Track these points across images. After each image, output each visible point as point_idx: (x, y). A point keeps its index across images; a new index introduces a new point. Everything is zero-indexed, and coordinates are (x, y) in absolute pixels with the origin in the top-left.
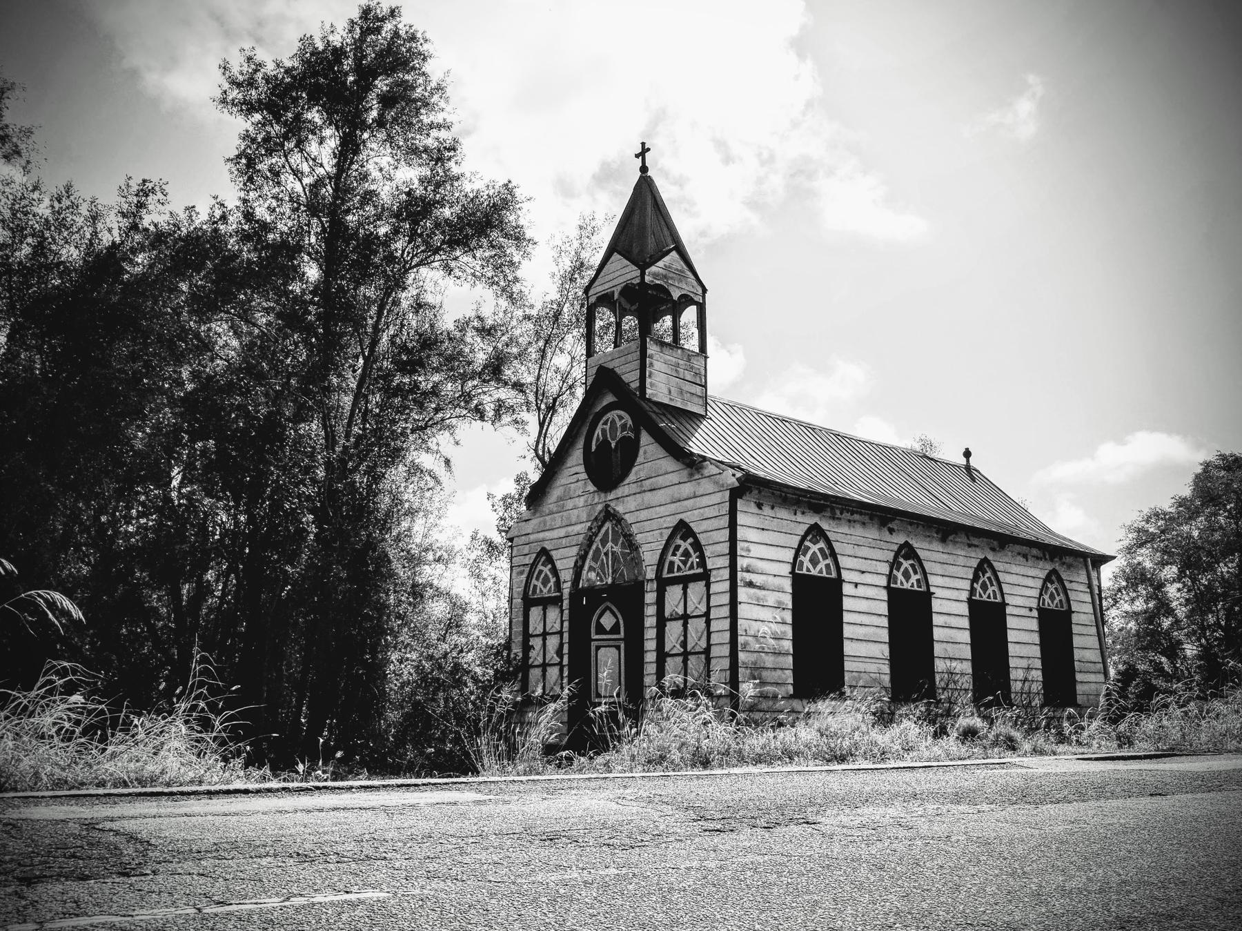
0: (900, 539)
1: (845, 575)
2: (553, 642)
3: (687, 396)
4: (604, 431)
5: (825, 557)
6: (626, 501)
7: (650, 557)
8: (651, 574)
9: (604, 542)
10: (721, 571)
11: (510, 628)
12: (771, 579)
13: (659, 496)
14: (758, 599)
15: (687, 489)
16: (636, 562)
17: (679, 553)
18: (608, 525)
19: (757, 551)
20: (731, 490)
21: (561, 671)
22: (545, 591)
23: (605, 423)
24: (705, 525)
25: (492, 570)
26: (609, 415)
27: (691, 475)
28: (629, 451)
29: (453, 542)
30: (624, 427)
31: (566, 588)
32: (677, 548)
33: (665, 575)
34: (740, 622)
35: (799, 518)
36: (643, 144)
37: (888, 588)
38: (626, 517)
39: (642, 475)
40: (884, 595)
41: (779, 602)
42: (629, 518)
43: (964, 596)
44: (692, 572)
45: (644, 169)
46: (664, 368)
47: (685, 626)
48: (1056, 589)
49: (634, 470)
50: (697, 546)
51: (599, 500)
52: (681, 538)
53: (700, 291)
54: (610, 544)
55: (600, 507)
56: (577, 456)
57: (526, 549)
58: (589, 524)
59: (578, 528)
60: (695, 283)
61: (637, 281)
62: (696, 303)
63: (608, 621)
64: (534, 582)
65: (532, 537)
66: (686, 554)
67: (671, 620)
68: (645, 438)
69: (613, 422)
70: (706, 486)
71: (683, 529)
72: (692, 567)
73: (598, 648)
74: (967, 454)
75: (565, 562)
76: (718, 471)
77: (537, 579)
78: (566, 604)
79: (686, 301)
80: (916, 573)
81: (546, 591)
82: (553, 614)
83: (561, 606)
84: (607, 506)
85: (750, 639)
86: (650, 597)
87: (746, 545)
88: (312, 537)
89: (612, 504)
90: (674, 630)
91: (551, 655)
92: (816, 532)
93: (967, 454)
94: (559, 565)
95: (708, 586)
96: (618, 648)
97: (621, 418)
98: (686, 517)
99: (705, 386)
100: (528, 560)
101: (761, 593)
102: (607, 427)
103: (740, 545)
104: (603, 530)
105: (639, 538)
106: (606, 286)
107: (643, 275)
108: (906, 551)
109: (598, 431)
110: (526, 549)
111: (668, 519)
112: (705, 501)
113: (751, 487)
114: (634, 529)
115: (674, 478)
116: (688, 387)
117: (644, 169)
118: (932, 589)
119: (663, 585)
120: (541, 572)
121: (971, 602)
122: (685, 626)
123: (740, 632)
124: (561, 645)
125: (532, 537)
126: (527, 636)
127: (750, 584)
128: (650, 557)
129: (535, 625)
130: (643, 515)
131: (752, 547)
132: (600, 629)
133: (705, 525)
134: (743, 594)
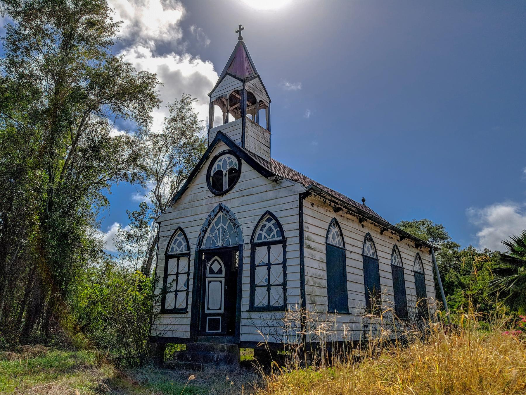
0: (366, 231)
1: (348, 247)
2: (183, 279)
3: (262, 151)
4: (219, 165)
5: (338, 236)
6: (231, 200)
7: (246, 232)
8: (247, 240)
9: (217, 223)
10: (293, 239)
11: (156, 270)
12: (317, 245)
13: (253, 198)
14: (312, 256)
15: (271, 194)
16: (239, 234)
17: (265, 229)
18: (220, 214)
19: (312, 229)
20: (300, 194)
21: (187, 294)
22: (179, 250)
23: (220, 161)
24: (283, 214)
25: (128, 247)
26: (223, 157)
27: (274, 187)
28: (234, 176)
29: (102, 239)
30: (231, 163)
31: (193, 249)
32: (264, 226)
33: (256, 241)
34: (305, 268)
35: (328, 214)
36: (240, 26)
38: (232, 210)
39: (243, 187)
40: (361, 258)
41: (321, 258)
42: (234, 211)
43: (389, 262)
44: (274, 239)
45: (240, 38)
46: (253, 135)
47: (269, 269)
49: (237, 185)
50: (279, 225)
51: (216, 201)
52: (267, 221)
53: (268, 101)
54: (221, 224)
55: (216, 205)
56: (201, 178)
57: (169, 228)
58: (209, 213)
59: (201, 216)
60: (266, 97)
61: (241, 88)
62: (265, 107)
63: (216, 267)
64: (172, 245)
65: (172, 222)
66: (270, 230)
67: (257, 266)
68: (246, 167)
69: (225, 161)
70: (283, 193)
71: (269, 215)
72: (273, 236)
73: (210, 282)
74: (364, 200)
75: (193, 236)
76: (291, 184)
77: (174, 243)
78: (192, 257)
81: (182, 249)
82: (184, 262)
83: (189, 259)
84: (220, 204)
85: (310, 278)
86: (247, 253)
87: (307, 225)
88: (37, 227)
89: (224, 203)
90: (261, 273)
91: (181, 286)
92: (335, 222)
93: (364, 200)
94: (189, 236)
95: (284, 247)
96: (221, 282)
97: (229, 158)
98: (271, 210)
99: (269, 148)
100: (170, 234)
101: (313, 252)
102: (221, 163)
103: (305, 224)
104: (217, 217)
105: (240, 221)
106: (219, 93)
107: (244, 86)
108: (369, 238)
109: (215, 165)
110: (169, 228)
111: (258, 210)
112: (283, 200)
113: (312, 192)
114: (237, 216)
115: (264, 189)
116: (263, 147)
117: (240, 38)
118: (379, 258)
119: (254, 246)
120: (177, 240)
121: (392, 265)
122: (269, 269)
123: (306, 274)
124: (188, 280)
125: (172, 222)
126: (166, 275)
127: (309, 247)
128: (246, 232)
129: (172, 270)
130: (243, 208)
131: (310, 226)
132: (212, 271)
133: (283, 214)
134: (306, 251)
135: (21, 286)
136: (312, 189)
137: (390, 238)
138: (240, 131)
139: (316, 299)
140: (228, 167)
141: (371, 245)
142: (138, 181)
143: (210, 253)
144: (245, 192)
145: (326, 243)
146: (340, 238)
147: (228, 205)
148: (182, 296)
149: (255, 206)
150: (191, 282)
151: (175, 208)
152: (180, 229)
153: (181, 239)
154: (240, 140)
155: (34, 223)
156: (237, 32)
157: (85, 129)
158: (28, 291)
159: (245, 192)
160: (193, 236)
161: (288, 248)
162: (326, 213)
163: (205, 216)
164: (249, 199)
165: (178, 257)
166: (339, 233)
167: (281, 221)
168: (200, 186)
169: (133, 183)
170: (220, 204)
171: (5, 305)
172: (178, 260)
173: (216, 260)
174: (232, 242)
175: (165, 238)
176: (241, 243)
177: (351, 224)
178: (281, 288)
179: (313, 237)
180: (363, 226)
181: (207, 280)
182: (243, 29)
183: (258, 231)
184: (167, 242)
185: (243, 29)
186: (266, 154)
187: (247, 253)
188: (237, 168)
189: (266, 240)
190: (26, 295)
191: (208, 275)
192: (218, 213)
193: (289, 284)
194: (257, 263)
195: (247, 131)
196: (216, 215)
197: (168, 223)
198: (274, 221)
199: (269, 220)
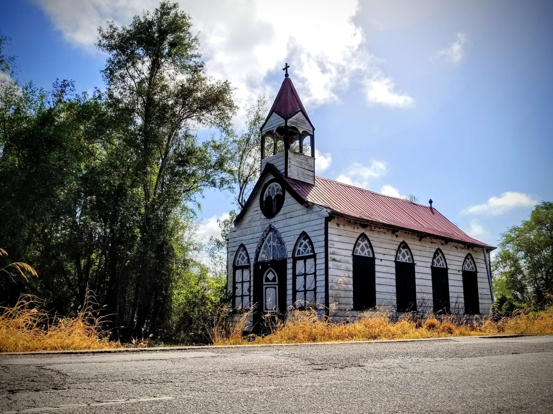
0: (401, 240)
1: (376, 256)
2: (246, 285)
3: (306, 176)
4: (269, 192)
5: (367, 248)
6: (278, 222)
7: (289, 248)
8: (290, 255)
9: (269, 241)
10: (321, 254)
12: (343, 257)
14: (337, 267)
15: (306, 217)
16: (283, 250)
17: (302, 246)
18: (271, 233)
20: (326, 218)
22: (243, 263)
23: (270, 188)
27: (308, 211)
28: (280, 200)
29: (202, 241)
31: (252, 262)
34: (329, 277)
35: (356, 230)
36: (286, 64)
37: (395, 261)
38: (279, 230)
39: (286, 211)
40: (393, 264)
41: (347, 268)
42: (280, 231)
43: (429, 265)
44: (308, 254)
45: (287, 75)
46: (296, 164)
47: (305, 278)
48: (470, 262)
49: (282, 209)
50: (311, 243)
51: (267, 222)
54: (272, 242)
56: (257, 203)
57: (234, 244)
58: (262, 233)
61: (284, 125)
63: (271, 276)
64: (238, 259)
65: (237, 239)
66: (306, 246)
68: (287, 195)
69: (273, 188)
70: (314, 216)
71: (304, 236)
72: (308, 252)
73: (266, 288)
74: (431, 202)
75: (252, 250)
76: (320, 209)
77: (239, 257)
78: (252, 268)
79: (305, 133)
80: (408, 255)
81: (243, 263)
82: (246, 272)
84: (270, 225)
85: (334, 284)
87: (332, 242)
88: (139, 239)
89: (273, 224)
90: (300, 280)
91: (246, 292)
93: (431, 202)
94: (249, 251)
95: (315, 261)
96: (275, 288)
97: (276, 186)
100: (236, 249)
102: (270, 190)
104: (269, 236)
105: (284, 240)
106: (270, 127)
107: (286, 122)
108: (403, 245)
109: (266, 192)
110: (234, 244)
111: (298, 231)
113: (333, 216)
115: (300, 213)
117: (287, 75)
118: (415, 262)
119: (295, 260)
120: (241, 254)
121: (432, 267)
122: (305, 278)
123: (329, 281)
124: (250, 287)
125: (237, 239)
126: (234, 283)
127: (334, 260)
128: (289, 248)
129: (238, 279)
131: (335, 243)
132: (267, 280)
134: (330, 264)
135: (131, 292)
136: (332, 214)
137: (432, 243)
138: (284, 162)
139: (341, 300)
140: (276, 194)
141: (406, 252)
142: (225, 186)
143: (265, 265)
144: (288, 215)
145: (353, 254)
146: (369, 249)
147: (276, 226)
148: (246, 299)
149: (295, 227)
150: (252, 289)
151: (239, 227)
152: (242, 245)
153: (243, 253)
154: (284, 171)
155: (135, 236)
156: (284, 69)
157: (172, 144)
158: (136, 295)
159: (288, 215)
160: (252, 250)
161: (318, 262)
162: (353, 230)
163: (259, 235)
164: (291, 222)
165: (242, 268)
166: (368, 245)
167: (313, 240)
168: (255, 209)
169: (221, 189)
170: (270, 225)
171: (120, 308)
172: (242, 271)
173: (271, 270)
174: (279, 256)
175: (232, 253)
176: (285, 257)
177: (382, 236)
178: (313, 292)
179: (339, 251)
180: (397, 236)
181: (264, 287)
182: (289, 67)
183: (298, 248)
184: (234, 256)
185: (289, 67)
186: (310, 178)
187: (290, 266)
188: (282, 194)
189: (303, 255)
190: (135, 299)
191: (264, 283)
192: (269, 232)
193: (318, 290)
194: (297, 273)
195: (290, 162)
196: (267, 235)
197: (233, 240)
198: (307, 240)
199: (305, 239)
